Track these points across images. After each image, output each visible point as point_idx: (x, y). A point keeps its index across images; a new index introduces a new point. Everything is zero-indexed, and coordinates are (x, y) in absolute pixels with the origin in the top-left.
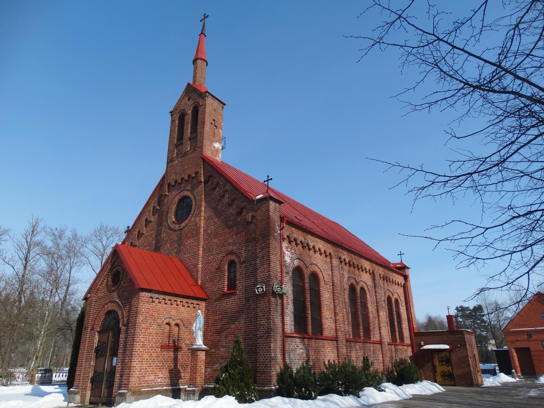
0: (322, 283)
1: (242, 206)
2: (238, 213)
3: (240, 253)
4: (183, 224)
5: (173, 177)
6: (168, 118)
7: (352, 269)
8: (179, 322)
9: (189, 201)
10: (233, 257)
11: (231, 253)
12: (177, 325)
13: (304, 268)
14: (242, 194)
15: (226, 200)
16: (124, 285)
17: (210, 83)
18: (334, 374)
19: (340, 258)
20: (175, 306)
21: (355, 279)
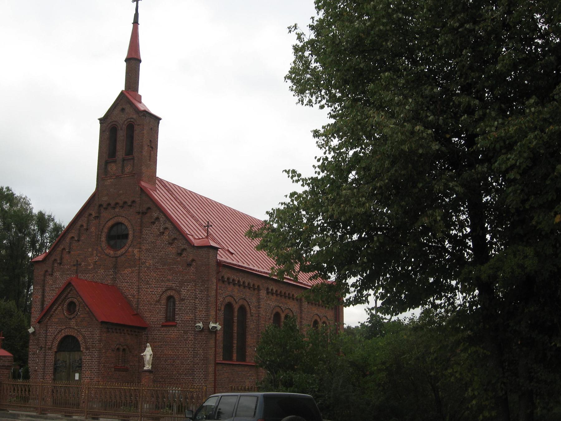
0: (249, 315)
1: (183, 247)
2: (178, 254)
3: (180, 291)
4: (119, 253)
5: (105, 198)
6: (97, 126)
7: (279, 298)
8: (125, 347)
9: (123, 227)
10: (170, 293)
11: (171, 289)
12: (124, 350)
13: (234, 303)
14: (183, 236)
15: (166, 237)
16: (82, 316)
17: (150, 99)
18: (337, 63)
19: (268, 289)
20: (123, 334)
21: (280, 307)
